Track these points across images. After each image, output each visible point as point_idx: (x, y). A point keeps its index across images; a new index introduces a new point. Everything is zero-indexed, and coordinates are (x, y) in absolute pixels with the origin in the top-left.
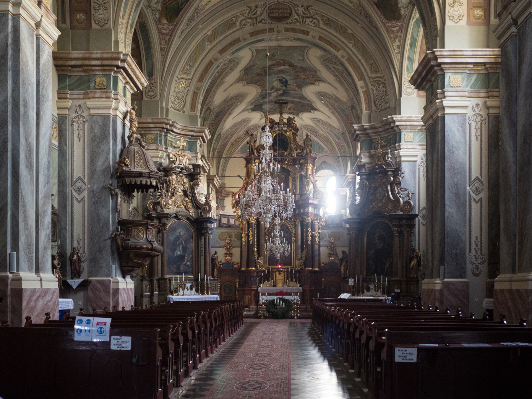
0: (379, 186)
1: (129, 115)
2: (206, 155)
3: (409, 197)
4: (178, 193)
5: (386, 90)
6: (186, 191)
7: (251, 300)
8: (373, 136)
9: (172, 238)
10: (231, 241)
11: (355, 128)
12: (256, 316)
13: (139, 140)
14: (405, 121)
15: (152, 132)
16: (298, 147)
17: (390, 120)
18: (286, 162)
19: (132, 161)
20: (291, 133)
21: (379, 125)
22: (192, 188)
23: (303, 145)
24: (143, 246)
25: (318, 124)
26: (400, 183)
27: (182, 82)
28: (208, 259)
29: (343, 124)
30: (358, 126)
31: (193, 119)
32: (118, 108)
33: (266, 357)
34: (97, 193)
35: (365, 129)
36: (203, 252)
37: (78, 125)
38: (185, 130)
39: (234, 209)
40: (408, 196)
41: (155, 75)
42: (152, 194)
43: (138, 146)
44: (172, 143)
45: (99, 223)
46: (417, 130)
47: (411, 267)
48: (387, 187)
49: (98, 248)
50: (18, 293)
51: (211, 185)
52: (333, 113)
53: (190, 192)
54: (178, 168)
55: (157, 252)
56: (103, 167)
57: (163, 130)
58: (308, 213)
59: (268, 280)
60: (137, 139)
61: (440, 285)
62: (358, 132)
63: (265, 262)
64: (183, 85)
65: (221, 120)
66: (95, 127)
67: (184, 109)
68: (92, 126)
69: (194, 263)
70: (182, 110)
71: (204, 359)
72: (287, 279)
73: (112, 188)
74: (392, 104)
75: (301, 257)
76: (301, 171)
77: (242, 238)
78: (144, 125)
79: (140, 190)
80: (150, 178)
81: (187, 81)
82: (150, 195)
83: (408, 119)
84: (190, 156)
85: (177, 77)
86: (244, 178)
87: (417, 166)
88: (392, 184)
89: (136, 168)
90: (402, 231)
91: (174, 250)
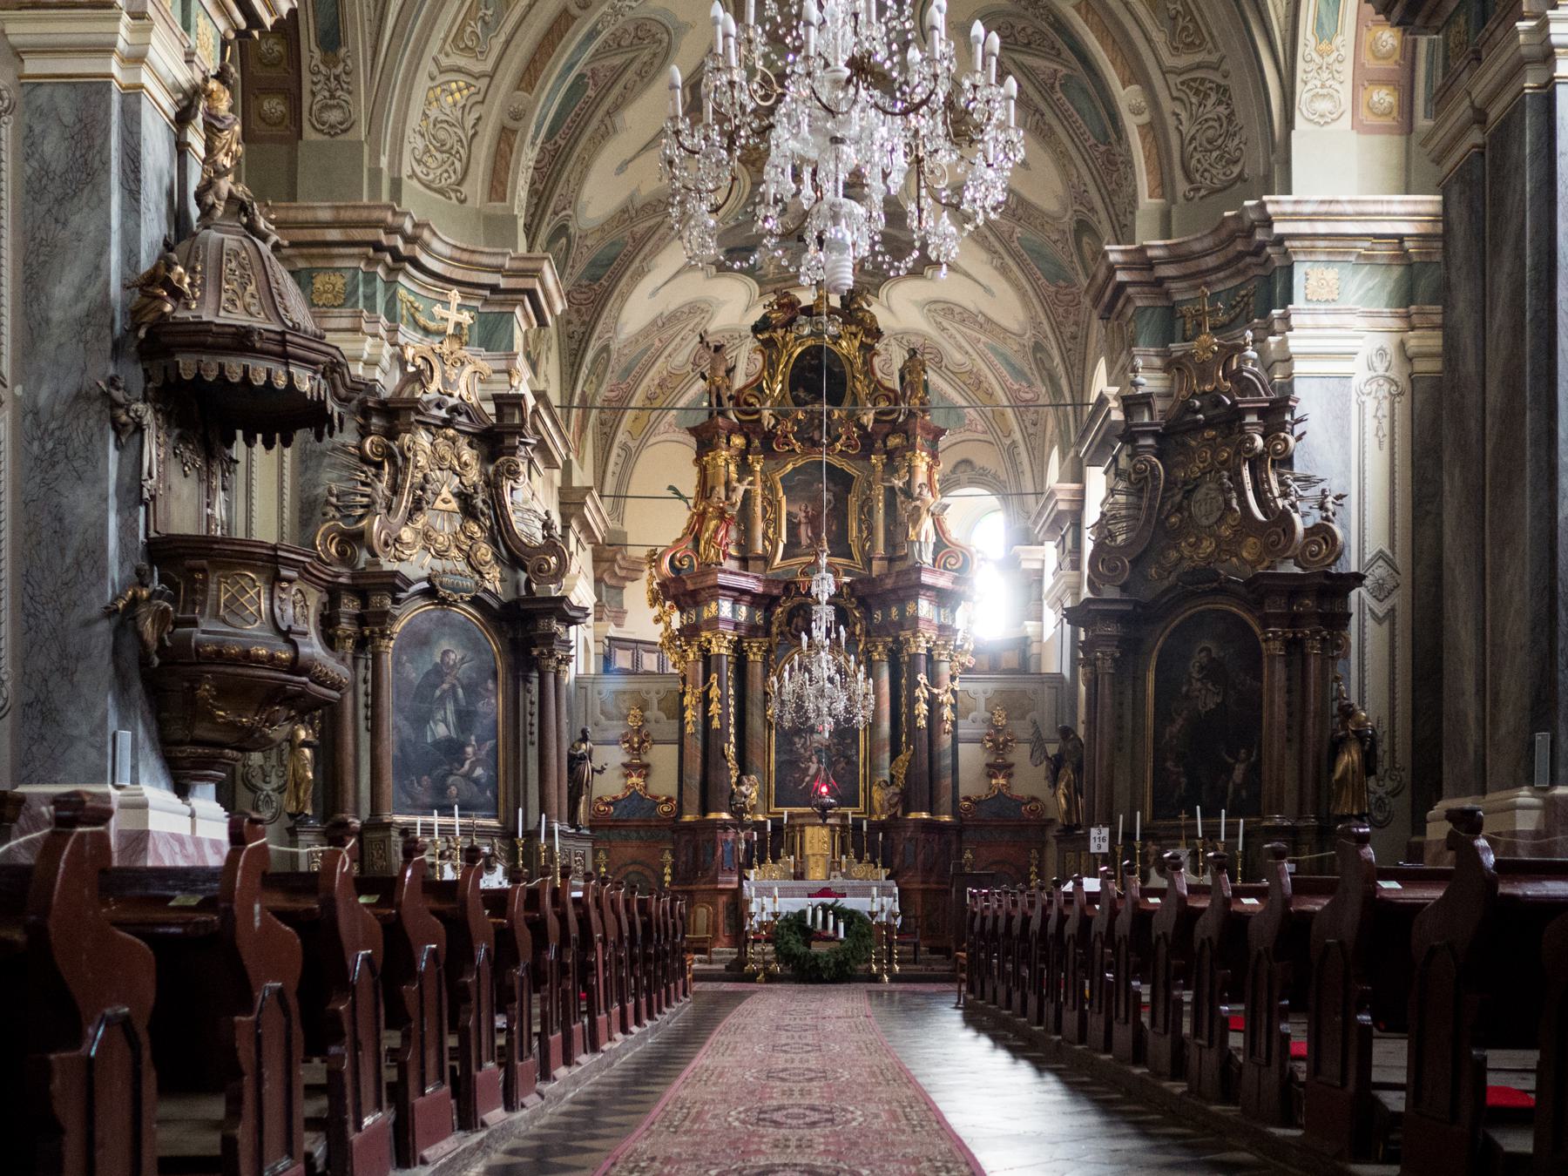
0: (1204, 474)
1: (202, 105)
2: (555, 399)
3: (1327, 510)
4: (439, 504)
5: (1232, 113)
6: (472, 497)
7: (715, 924)
8: (1180, 291)
9: (414, 673)
10: (645, 720)
11: (1113, 257)
12: (738, 972)
13: (243, 208)
14: (1311, 218)
15: (338, 264)
16: (879, 391)
17: (1253, 216)
18: (838, 446)
19: (210, 288)
20: (857, 343)
21: (1208, 243)
22: (493, 486)
23: (896, 384)
24: (253, 650)
25: (945, 324)
26: (1286, 461)
27: (454, 85)
28: (553, 752)
29: (1039, 308)
30: (1122, 252)
31: (497, 228)
32: (145, 55)
33: (813, 1124)
34: (53, 417)
35: (1150, 264)
36: (536, 729)
38: (467, 263)
39: (657, 610)
40: (1322, 507)
41: (346, 44)
42: (334, 500)
43: (238, 233)
44: (417, 315)
45: (62, 550)
46: (1352, 258)
47: (1337, 775)
48: (1240, 474)
49: (54, 656)
51: (574, 524)
52: (1003, 270)
53: (484, 502)
54: (439, 406)
55: (322, 684)
56: (80, 308)
57: (380, 255)
58: (916, 619)
59: (776, 858)
60: (238, 207)
61: (1536, 814)
62: (1121, 276)
63: (764, 795)
64: (457, 95)
65: (607, 294)
66: (44, 134)
67: (465, 189)
68: (31, 129)
69: (501, 773)
70: (456, 191)
71: (436, 1137)
72: (844, 851)
73: (119, 396)
74: (1254, 163)
75: (892, 776)
76: (892, 475)
77: (683, 709)
78: (305, 231)
79: (259, 436)
80: (285, 357)
81: (472, 81)
82: (328, 503)
83: (1324, 208)
84: (486, 367)
85: (435, 60)
86: (691, 502)
87: (1354, 397)
88: (1257, 463)
89: (222, 313)
90: (1301, 639)
91: (421, 721)
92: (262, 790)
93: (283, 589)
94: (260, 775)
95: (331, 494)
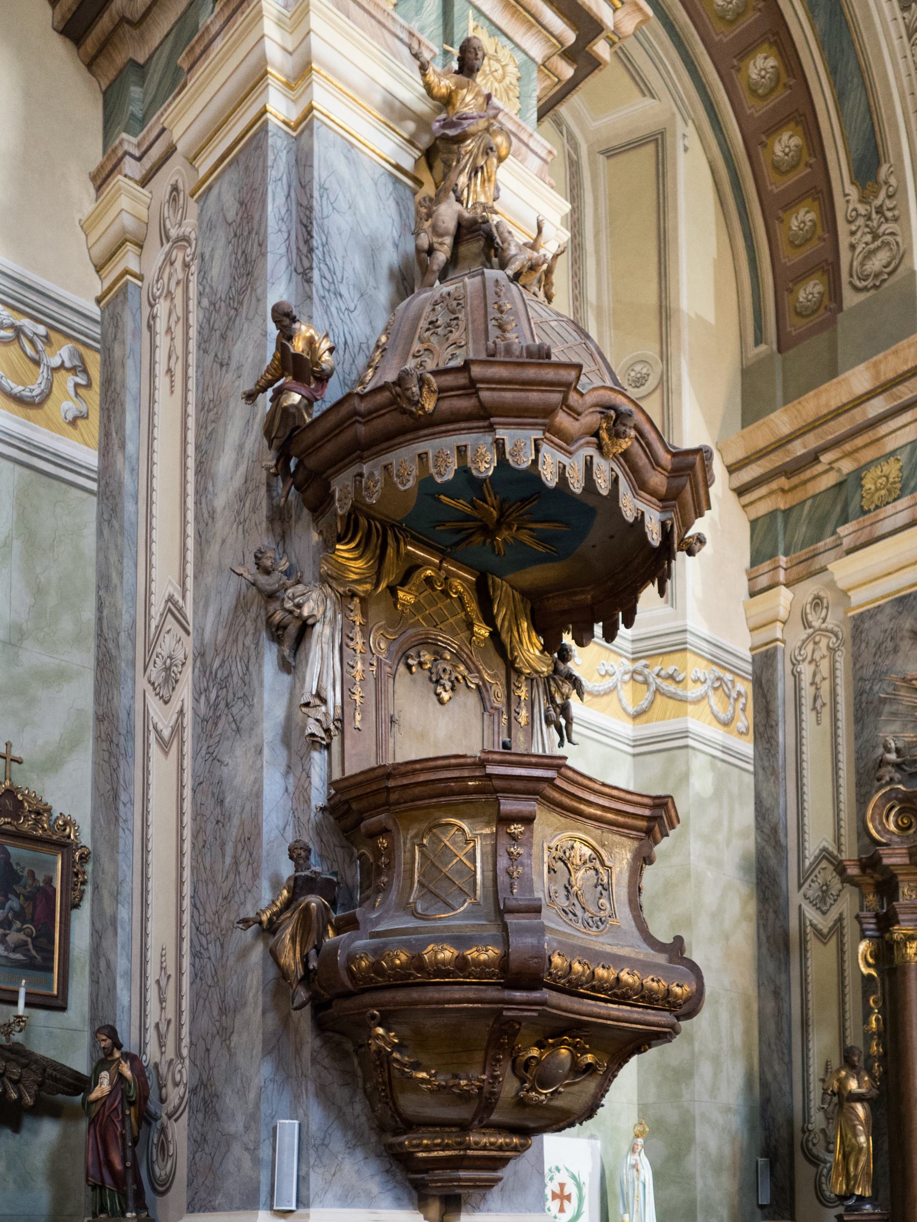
37: (812, 667)
50: (18, 1043)
92: (825, 1162)
93: (513, 837)
94: (822, 1143)
95: (888, 751)
